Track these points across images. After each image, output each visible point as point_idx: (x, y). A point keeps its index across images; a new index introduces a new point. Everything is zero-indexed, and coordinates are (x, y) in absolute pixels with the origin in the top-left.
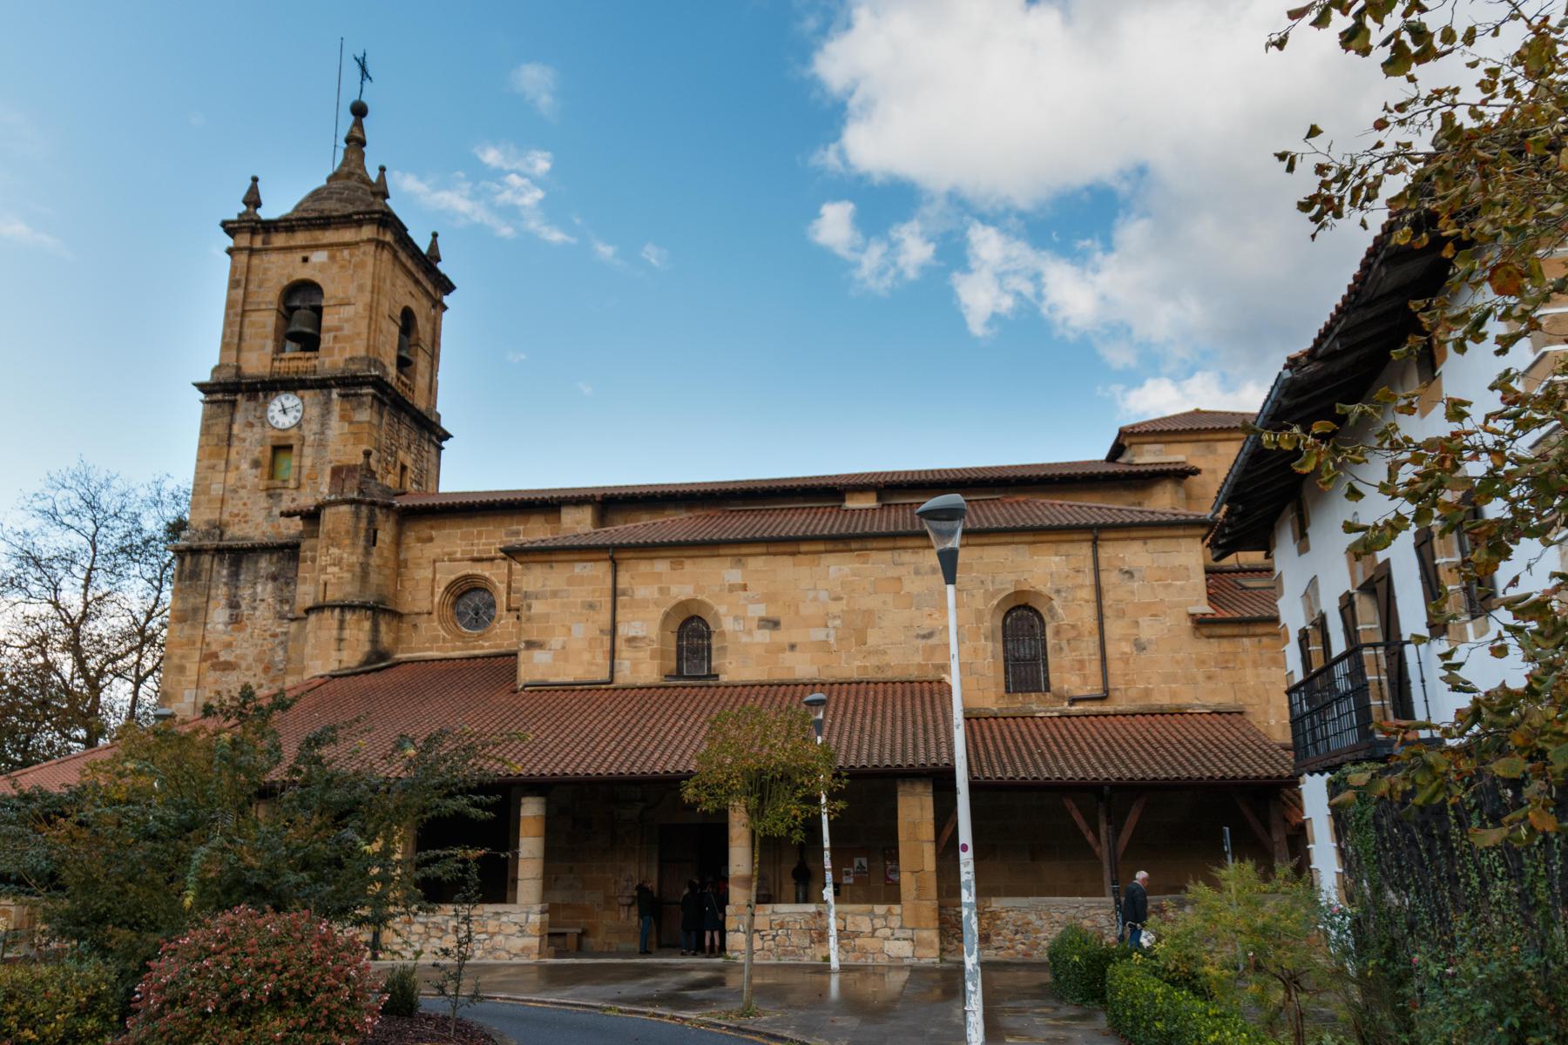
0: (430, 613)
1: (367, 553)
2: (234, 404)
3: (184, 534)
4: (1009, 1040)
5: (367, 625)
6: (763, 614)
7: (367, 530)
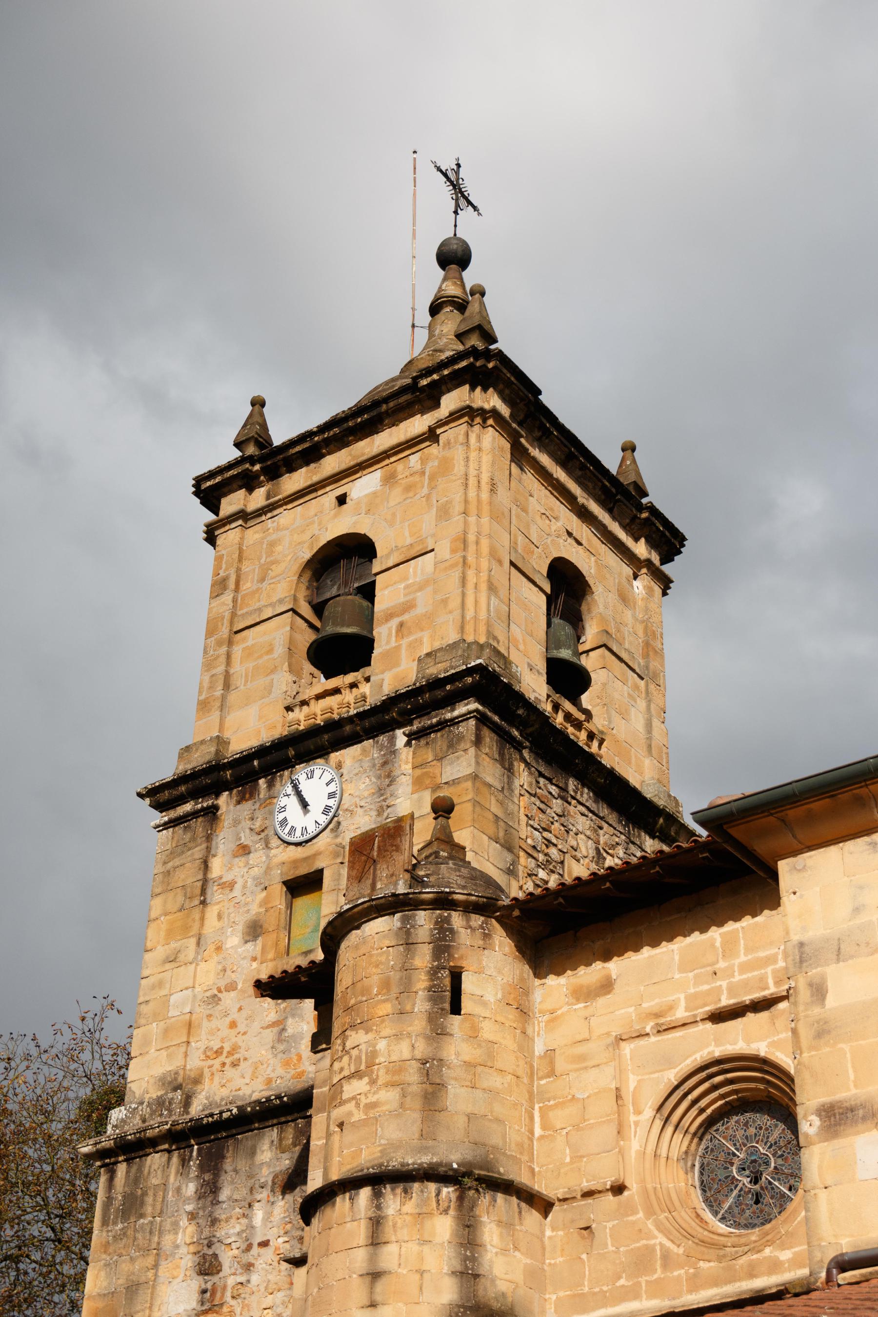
0: (618, 1189)
1: (438, 1033)
2: (212, 813)
3: (116, 1115)
5: (444, 1227)
7: (433, 973)
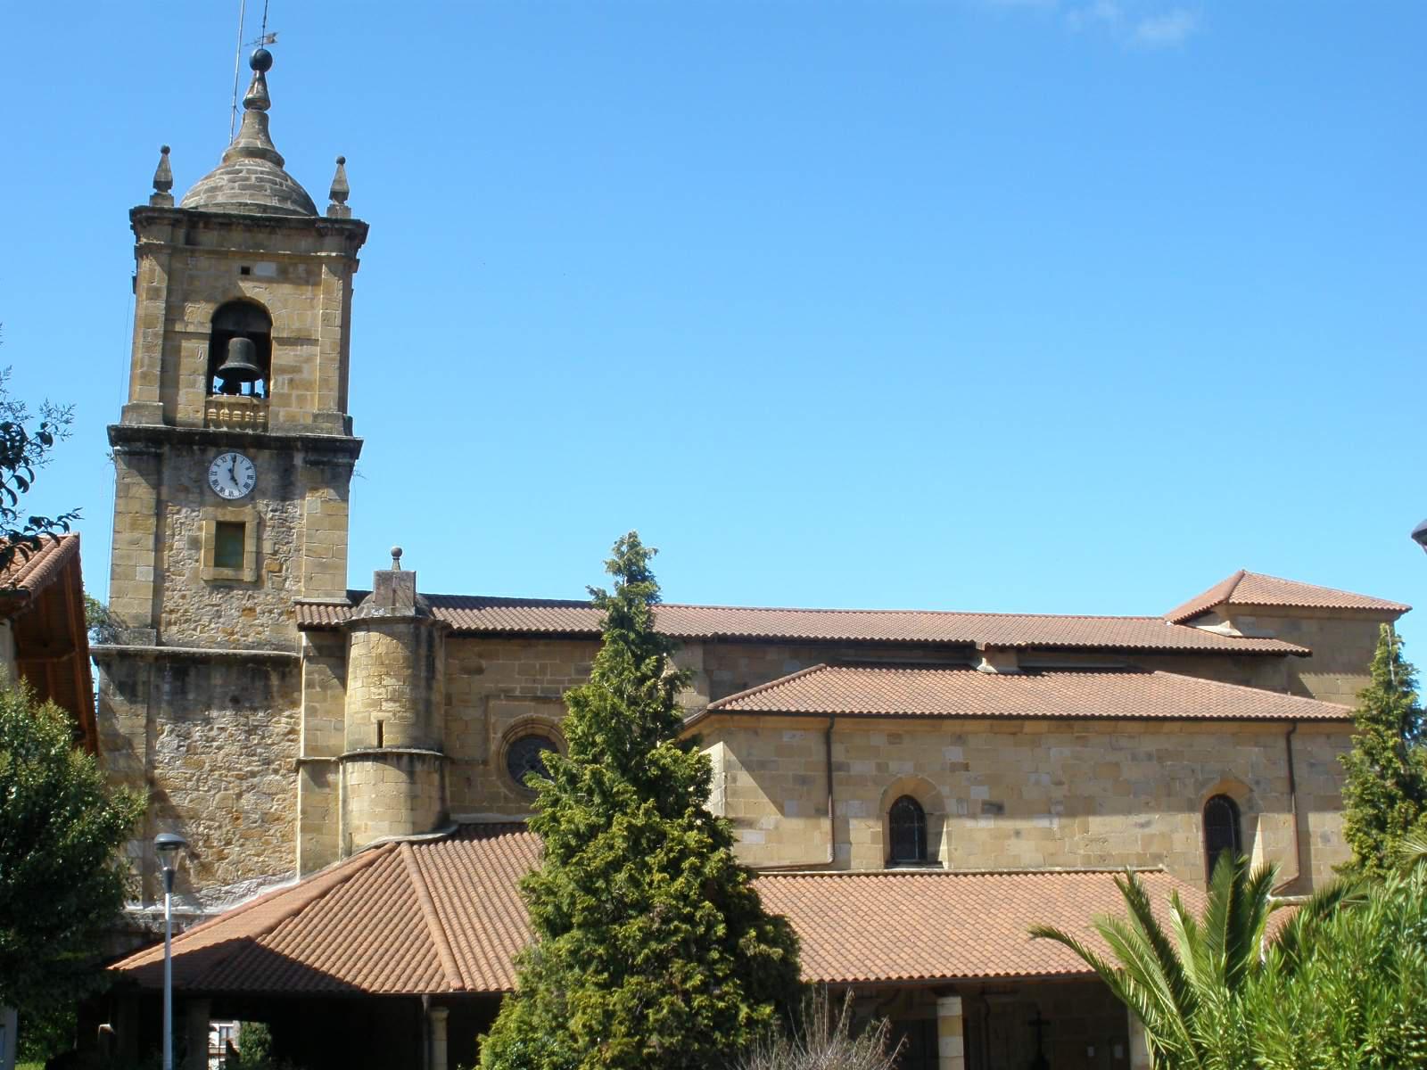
4: (11, 1017)
6: (986, 797)
